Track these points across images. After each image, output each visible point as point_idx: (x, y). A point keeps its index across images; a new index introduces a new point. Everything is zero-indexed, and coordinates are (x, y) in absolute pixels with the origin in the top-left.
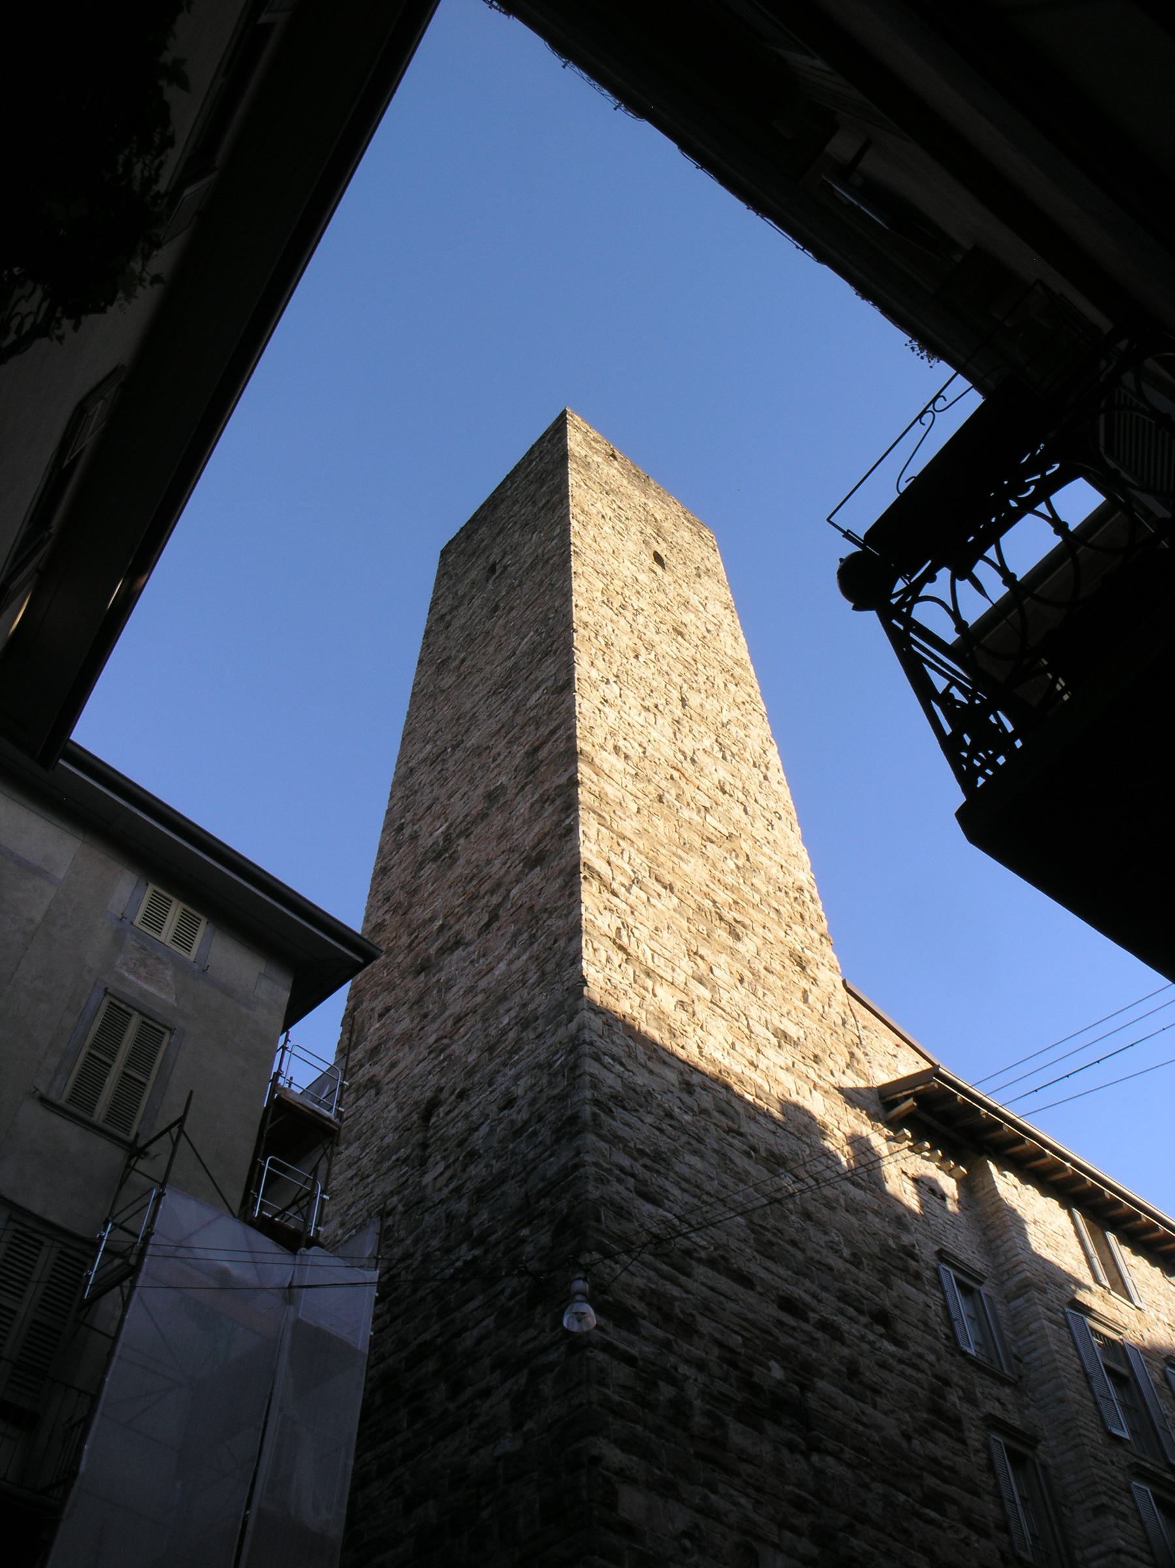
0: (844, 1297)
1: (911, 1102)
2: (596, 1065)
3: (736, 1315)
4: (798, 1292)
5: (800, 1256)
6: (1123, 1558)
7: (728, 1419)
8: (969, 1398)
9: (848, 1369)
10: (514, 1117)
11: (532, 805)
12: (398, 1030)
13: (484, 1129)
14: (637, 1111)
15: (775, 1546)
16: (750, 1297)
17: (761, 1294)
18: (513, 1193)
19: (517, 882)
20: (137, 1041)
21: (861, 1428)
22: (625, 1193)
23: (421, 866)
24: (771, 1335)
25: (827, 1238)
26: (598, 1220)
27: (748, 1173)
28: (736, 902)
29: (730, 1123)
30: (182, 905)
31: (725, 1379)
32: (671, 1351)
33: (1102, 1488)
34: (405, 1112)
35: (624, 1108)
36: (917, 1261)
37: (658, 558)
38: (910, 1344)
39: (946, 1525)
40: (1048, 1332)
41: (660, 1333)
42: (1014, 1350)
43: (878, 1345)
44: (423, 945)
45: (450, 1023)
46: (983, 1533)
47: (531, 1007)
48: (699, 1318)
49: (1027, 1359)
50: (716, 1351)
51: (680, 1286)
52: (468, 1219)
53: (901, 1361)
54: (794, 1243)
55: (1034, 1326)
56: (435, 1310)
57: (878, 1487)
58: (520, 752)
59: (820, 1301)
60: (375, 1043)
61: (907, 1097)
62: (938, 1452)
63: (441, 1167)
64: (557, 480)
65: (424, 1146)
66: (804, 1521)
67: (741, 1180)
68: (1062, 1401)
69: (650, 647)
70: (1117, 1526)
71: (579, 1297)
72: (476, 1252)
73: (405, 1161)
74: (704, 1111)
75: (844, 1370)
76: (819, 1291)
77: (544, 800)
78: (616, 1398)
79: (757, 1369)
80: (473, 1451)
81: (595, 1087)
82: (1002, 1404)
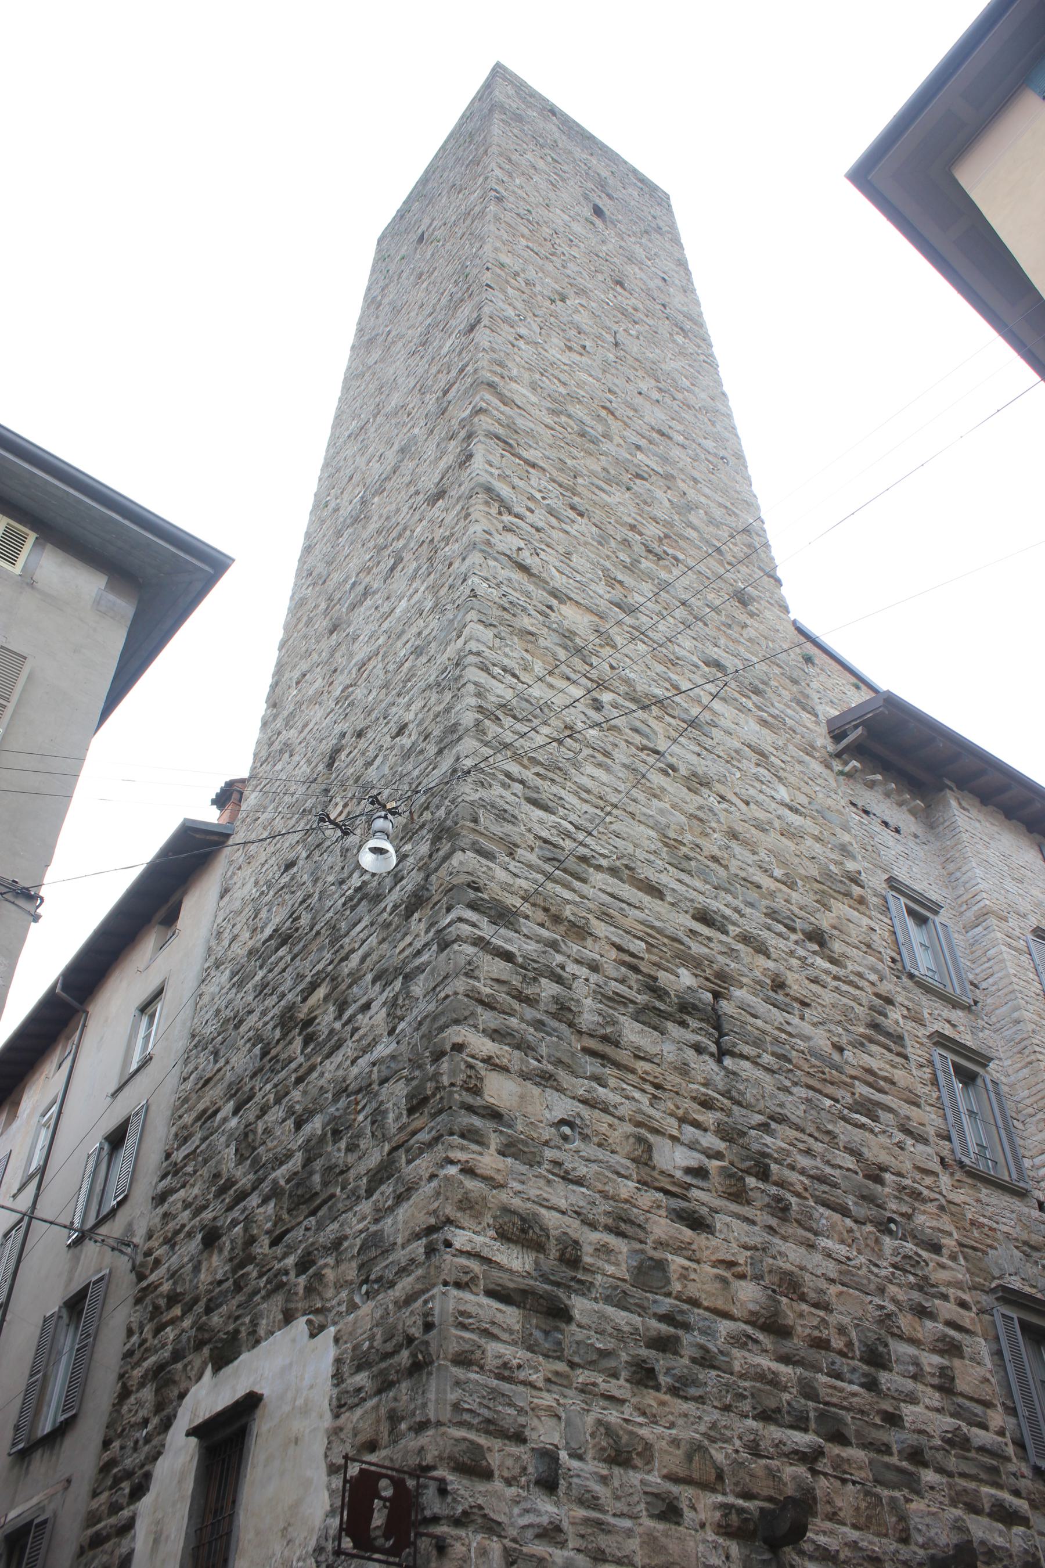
0: (772, 914)
1: (860, 730)
2: (485, 675)
3: (641, 923)
4: (715, 905)
7: (622, 1019)
9: (773, 981)
13: (379, 760)
15: (674, 1139)
16: (656, 905)
17: (672, 904)
19: (421, 520)
21: (784, 1036)
22: (511, 798)
23: (339, 534)
24: (682, 944)
25: (756, 858)
26: (475, 820)
27: (663, 790)
28: (666, 536)
31: (622, 981)
32: (558, 952)
35: (514, 717)
36: (863, 887)
37: (598, 211)
38: (849, 964)
39: (877, 1130)
40: (1005, 955)
41: (545, 933)
42: (971, 977)
43: (810, 961)
44: (338, 607)
45: (354, 671)
46: (921, 1139)
48: (594, 922)
49: (984, 985)
50: (613, 954)
51: (574, 891)
53: (836, 978)
57: (801, 1092)
58: (431, 399)
59: (742, 916)
61: (856, 727)
62: (875, 1064)
66: (709, 1118)
67: (655, 796)
68: (1018, 1022)
69: (582, 292)
75: (768, 981)
76: (742, 906)
78: (488, 990)
79: (662, 975)
80: (353, 1062)
81: (479, 695)
82: (954, 1026)
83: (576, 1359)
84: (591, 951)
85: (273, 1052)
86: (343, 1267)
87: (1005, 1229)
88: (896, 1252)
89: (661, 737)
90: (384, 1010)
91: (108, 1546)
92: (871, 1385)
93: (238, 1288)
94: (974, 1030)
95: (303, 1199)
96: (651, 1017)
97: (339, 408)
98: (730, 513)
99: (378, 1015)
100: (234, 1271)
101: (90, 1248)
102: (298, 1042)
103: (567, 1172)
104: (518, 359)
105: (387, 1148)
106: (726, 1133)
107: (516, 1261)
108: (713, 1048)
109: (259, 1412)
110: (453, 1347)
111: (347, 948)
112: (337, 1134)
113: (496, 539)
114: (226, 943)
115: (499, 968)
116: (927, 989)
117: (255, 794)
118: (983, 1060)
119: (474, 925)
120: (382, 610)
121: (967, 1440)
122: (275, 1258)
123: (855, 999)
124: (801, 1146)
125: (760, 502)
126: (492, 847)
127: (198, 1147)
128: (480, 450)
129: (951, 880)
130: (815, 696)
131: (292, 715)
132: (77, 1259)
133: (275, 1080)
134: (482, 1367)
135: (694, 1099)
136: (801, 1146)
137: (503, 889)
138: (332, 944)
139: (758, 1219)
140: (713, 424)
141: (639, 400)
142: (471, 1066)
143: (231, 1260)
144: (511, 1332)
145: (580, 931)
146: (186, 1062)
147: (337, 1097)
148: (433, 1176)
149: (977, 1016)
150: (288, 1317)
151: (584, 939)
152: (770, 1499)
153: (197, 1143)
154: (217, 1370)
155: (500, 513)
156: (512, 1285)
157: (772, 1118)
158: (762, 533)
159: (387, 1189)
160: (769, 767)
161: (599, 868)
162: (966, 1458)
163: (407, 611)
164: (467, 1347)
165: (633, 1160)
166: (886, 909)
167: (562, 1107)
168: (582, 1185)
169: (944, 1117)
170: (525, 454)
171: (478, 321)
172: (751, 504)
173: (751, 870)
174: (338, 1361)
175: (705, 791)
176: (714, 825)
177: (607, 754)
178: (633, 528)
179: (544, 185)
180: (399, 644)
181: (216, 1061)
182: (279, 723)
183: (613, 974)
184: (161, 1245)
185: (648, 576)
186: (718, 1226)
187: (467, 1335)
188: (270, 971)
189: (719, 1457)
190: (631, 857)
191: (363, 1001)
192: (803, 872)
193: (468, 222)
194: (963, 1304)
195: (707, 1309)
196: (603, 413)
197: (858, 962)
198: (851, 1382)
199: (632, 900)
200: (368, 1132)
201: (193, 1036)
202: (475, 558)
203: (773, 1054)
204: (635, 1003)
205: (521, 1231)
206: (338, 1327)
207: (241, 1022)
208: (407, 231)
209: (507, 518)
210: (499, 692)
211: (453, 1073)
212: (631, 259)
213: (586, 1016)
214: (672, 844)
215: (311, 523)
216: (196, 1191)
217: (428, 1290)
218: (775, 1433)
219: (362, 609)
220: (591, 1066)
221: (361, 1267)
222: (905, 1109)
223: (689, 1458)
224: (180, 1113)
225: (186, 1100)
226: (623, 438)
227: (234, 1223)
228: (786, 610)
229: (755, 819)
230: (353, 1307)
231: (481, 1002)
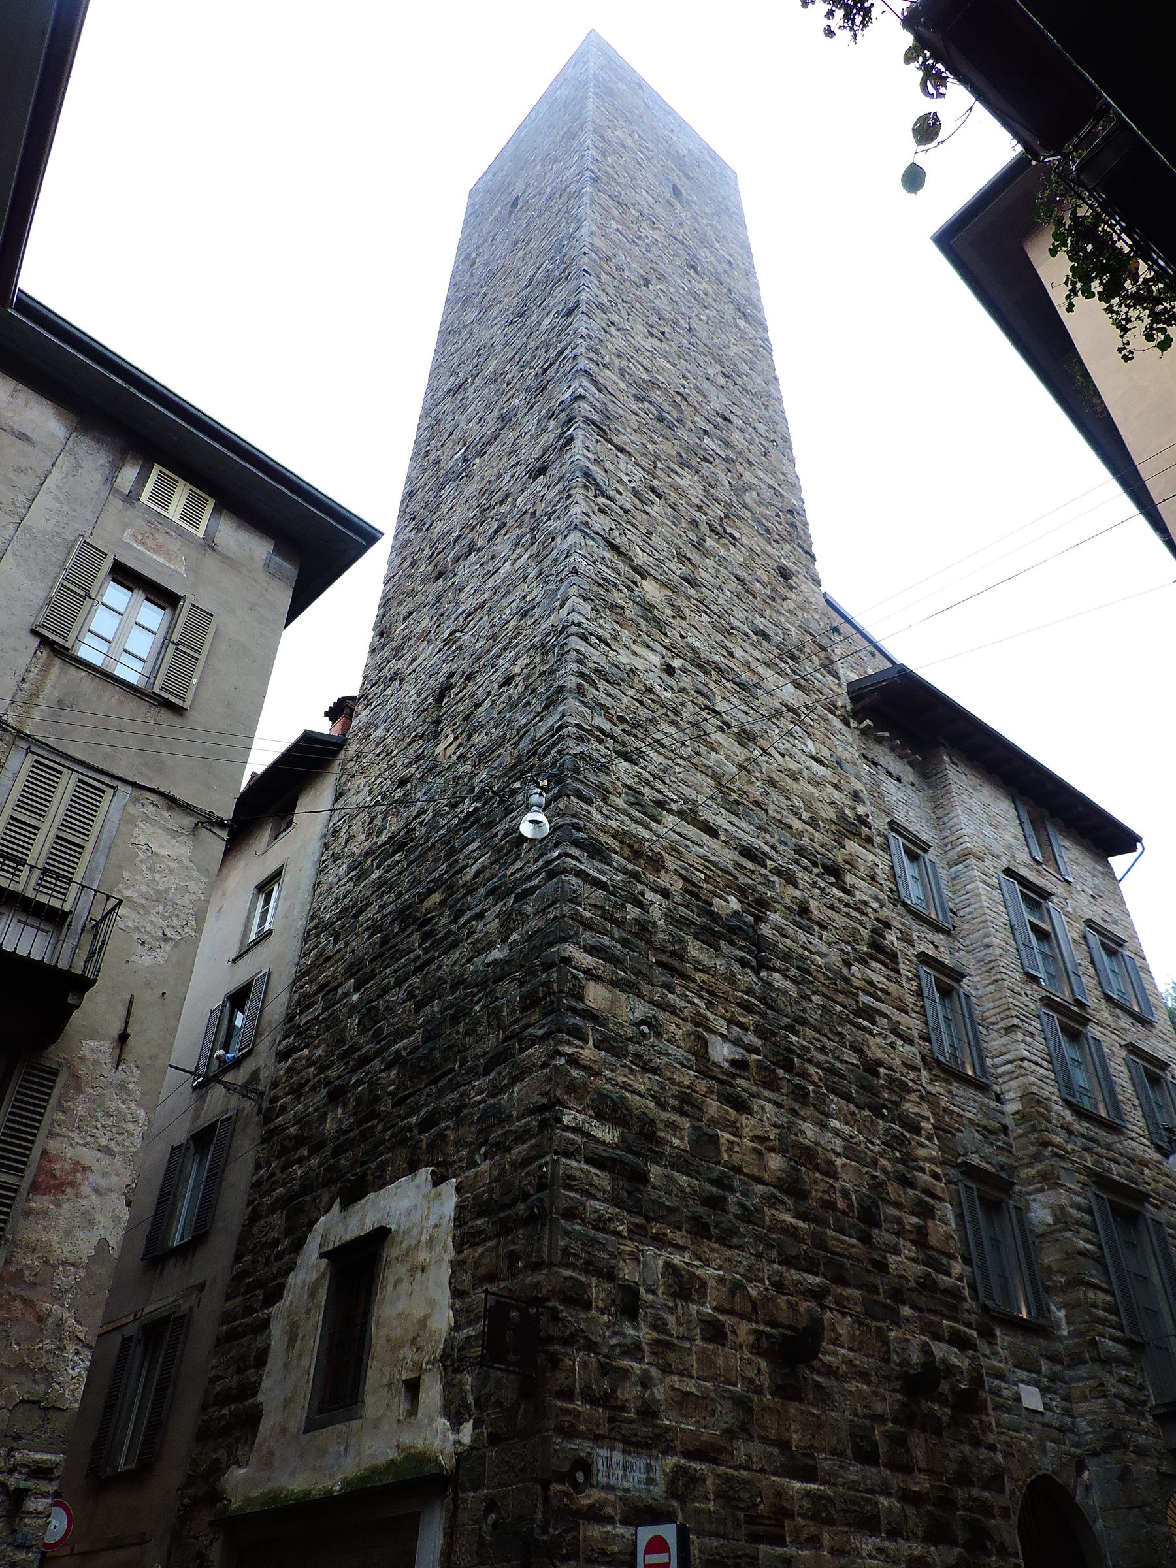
4: (758, 843)
6: (1026, 1064)
8: (905, 938)
10: (511, 691)
11: (539, 421)
12: (419, 629)
13: (487, 703)
14: (619, 684)
15: (722, 1036)
16: (714, 843)
18: (507, 754)
21: (806, 953)
22: (604, 751)
24: (732, 875)
25: (789, 803)
29: (706, 702)
32: (640, 882)
33: (1014, 1013)
34: (423, 697)
35: (608, 681)
37: (676, 192)
38: (857, 893)
40: (981, 891)
41: (630, 866)
42: (951, 906)
45: (461, 619)
46: (909, 1041)
49: (961, 913)
51: (651, 830)
52: (471, 779)
53: (847, 905)
56: (442, 854)
60: (400, 641)
62: (875, 978)
63: (451, 738)
67: (713, 749)
68: (988, 946)
69: (661, 278)
70: (1023, 1041)
71: (535, 808)
73: (421, 737)
74: (683, 690)
77: (551, 416)
78: (588, 914)
79: (716, 900)
81: (580, 662)
82: (936, 947)
83: (651, 1214)
84: (664, 880)
86: (462, 1131)
87: (968, 1115)
88: (887, 1131)
89: (718, 698)
90: (497, 920)
91: (245, 1341)
92: (865, 1239)
93: (363, 1137)
94: (952, 951)
95: (423, 1068)
97: (435, 360)
98: (777, 494)
99: (491, 925)
100: (359, 1123)
101: (218, 1091)
103: (645, 1063)
104: (609, 346)
106: (760, 1032)
107: (607, 1134)
108: (754, 962)
109: (388, 1242)
110: (563, 1204)
112: (455, 1020)
117: (367, 711)
118: (959, 976)
119: (576, 859)
120: (487, 568)
121: (935, 1282)
122: (399, 1116)
123: (861, 924)
124: (817, 1044)
125: (801, 482)
126: (587, 792)
127: (320, 1014)
128: (581, 436)
129: (939, 823)
131: (401, 647)
132: (201, 1099)
133: (396, 966)
134: (583, 1220)
135: (738, 1004)
136: (817, 1044)
137: (599, 829)
139: (784, 1103)
140: (766, 407)
141: (706, 385)
142: (575, 977)
143: (356, 1114)
144: (605, 1192)
146: (306, 939)
148: (545, 1065)
149: (955, 939)
150: (413, 1168)
151: (658, 871)
152: (790, 1327)
153: (320, 1011)
154: (344, 1207)
155: (595, 496)
156: (606, 1155)
157: (795, 1021)
158: (801, 513)
159: (503, 1070)
160: (800, 723)
161: (670, 811)
162: (934, 1298)
164: (572, 1204)
165: (693, 1054)
166: (886, 848)
167: (642, 1010)
168: (656, 1074)
169: (926, 1023)
170: (615, 439)
173: (785, 813)
174: (460, 1207)
176: (757, 774)
178: (699, 508)
180: (505, 602)
181: (335, 943)
182: (387, 652)
184: (286, 1095)
186: (755, 1108)
187: (572, 1194)
188: (387, 872)
189: (753, 1293)
190: (694, 802)
191: (478, 910)
192: (824, 815)
194: (936, 1176)
195: (745, 1175)
196: (678, 399)
197: (864, 891)
198: (850, 1236)
199: (695, 839)
201: (313, 918)
203: (798, 968)
204: (695, 924)
205: (609, 1109)
206: (460, 1179)
207: (360, 912)
209: (601, 500)
210: (595, 659)
211: (560, 981)
213: (660, 935)
215: (412, 469)
216: (320, 1052)
217: (542, 1157)
218: (795, 1275)
219: (468, 562)
220: (659, 975)
221: (479, 1132)
222: (897, 1016)
223: (732, 1294)
224: (301, 983)
226: (694, 422)
227: (359, 1083)
228: (818, 583)
229: (789, 770)
230: (473, 1164)
231: (582, 924)
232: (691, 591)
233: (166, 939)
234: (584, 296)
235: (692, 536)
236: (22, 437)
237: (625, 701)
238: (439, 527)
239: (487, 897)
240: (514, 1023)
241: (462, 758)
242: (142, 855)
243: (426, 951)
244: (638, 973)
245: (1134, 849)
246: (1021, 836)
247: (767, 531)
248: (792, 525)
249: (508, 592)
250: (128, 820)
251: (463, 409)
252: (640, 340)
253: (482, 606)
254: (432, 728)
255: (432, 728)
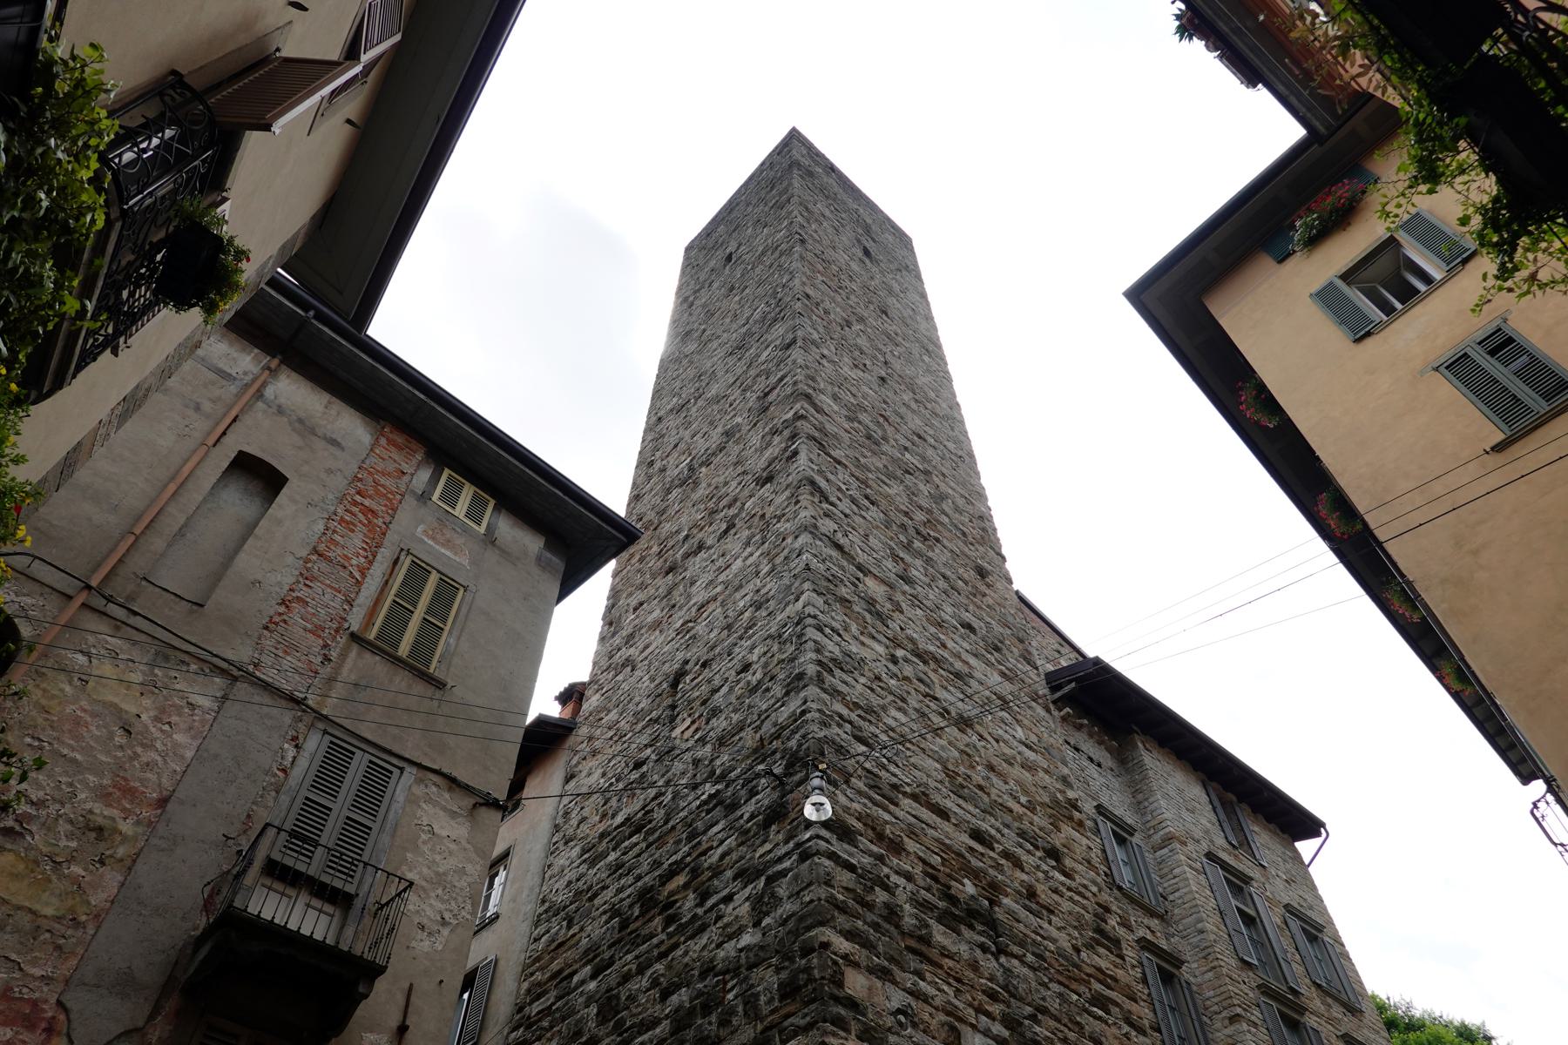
0: (1022, 834)
1: (1073, 685)
4: (984, 826)
5: (986, 799)
7: (931, 922)
8: (1125, 924)
12: (650, 619)
15: (973, 1026)
18: (749, 739)
20: (435, 593)
23: (669, 491)
30: (473, 488)
31: (928, 890)
37: (867, 252)
41: (875, 849)
45: (694, 610)
47: (763, 592)
48: (906, 839)
49: (1171, 898)
52: (712, 761)
53: (1069, 889)
54: (981, 788)
55: (1176, 871)
57: (1055, 987)
58: (752, 397)
60: (630, 630)
61: (1070, 682)
62: (1103, 964)
63: (688, 721)
64: (785, 183)
65: (673, 707)
66: (996, 1009)
68: (1201, 932)
69: (861, 320)
72: (719, 787)
73: (656, 721)
74: (906, 678)
77: (774, 432)
79: (953, 883)
80: (719, 946)
81: (818, 651)
85: (632, 927)
94: (1168, 936)
96: (950, 920)
98: (969, 503)
99: (741, 908)
102: (658, 921)
105: (760, 1027)
108: (993, 949)
111: (705, 846)
113: (820, 523)
114: (574, 822)
115: (845, 877)
116: (1132, 900)
117: (598, 696)
119: (827, 841)
123: (1084, 908)
128: (802, 446)
129: (1139, 807)
130: (1035, 653)
131: (631, 636)
133: (636, 952)
135: (984, 992)
138: (690, 839)
141: (903, 410)
142: (835, 963)
145: (897, 848)
146: (537, 924)
147: (703, 975)
158: (990, 519)
161: (905, 794)
163: (742, 570)
167: (898, 999)
171: (794, 341)
172: (981, 495)
175: (969, 731)
177: (903, 700)
178: (906, 514)
179: (830, 230)
180: (738, 595)
181: (569, 927)
182: (617, 640)
183: (922, 884)
185: (918, 554)
193: (777, 254)
197: (1084, 876)
200: (740, 1009)
201: (543, 902)
202: (804, 538)
203: (1034, 954)
207: (595, 895)
208: (715, 247)
209: (825, 505)
211: (823, 967)
212: (890, 291)
213: (907, 919)
214: (951, 775)
219: (698, 558)
220: (913, 962)
225: (538, 959)
228: (1010, 581)
231: (837, 907)
232: (906, 588)
233: (444, 922)
234: (799, 333)
235: (902, 538)
236: (334, 442)
237: (858, 689)
238: (667, 527)
239: (735, 879)
240: (772, 1012)
241: (702, 741)
242: (424, 837)
243: (670, 936)
244: (891, 959)
245: (1319, 835)
246: (1214, 820)
247: (964, 534)
248: (984, 530)
249: (741, 586)
250: (412, 801)
251: (687, 425)
252: (846, 371)
253: (715, 599)
254: (668, 712)
255: (668, 712)
